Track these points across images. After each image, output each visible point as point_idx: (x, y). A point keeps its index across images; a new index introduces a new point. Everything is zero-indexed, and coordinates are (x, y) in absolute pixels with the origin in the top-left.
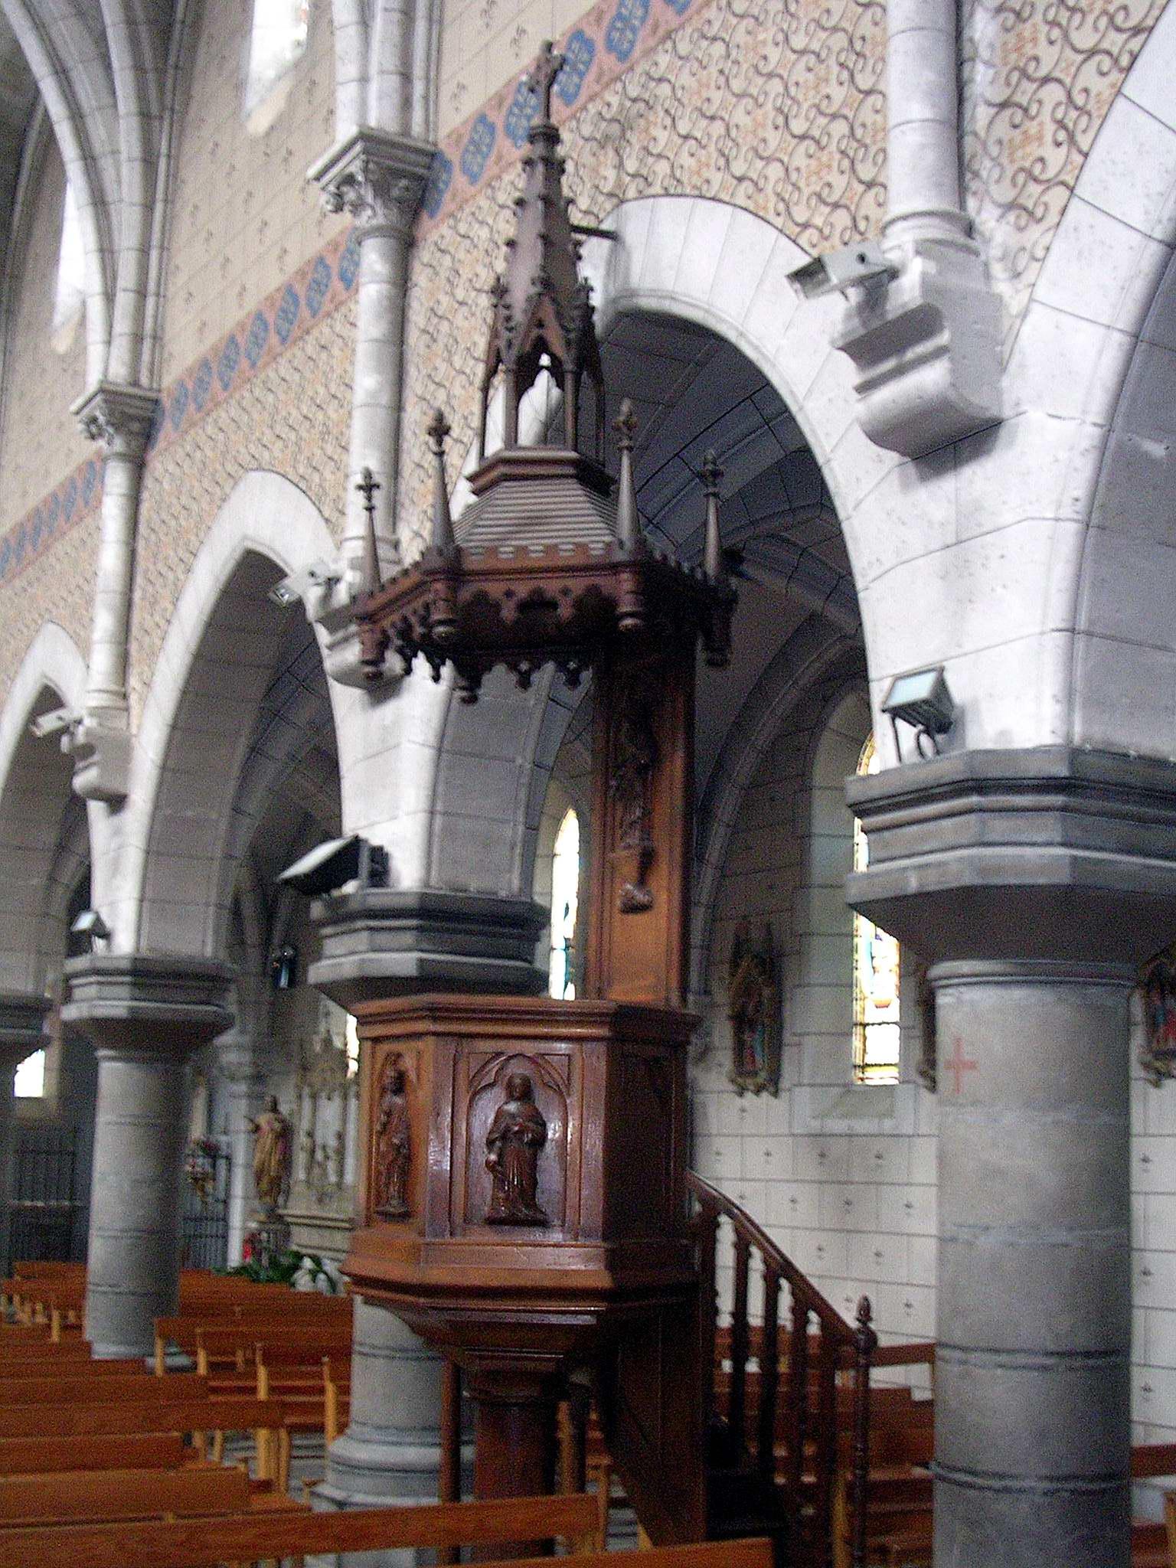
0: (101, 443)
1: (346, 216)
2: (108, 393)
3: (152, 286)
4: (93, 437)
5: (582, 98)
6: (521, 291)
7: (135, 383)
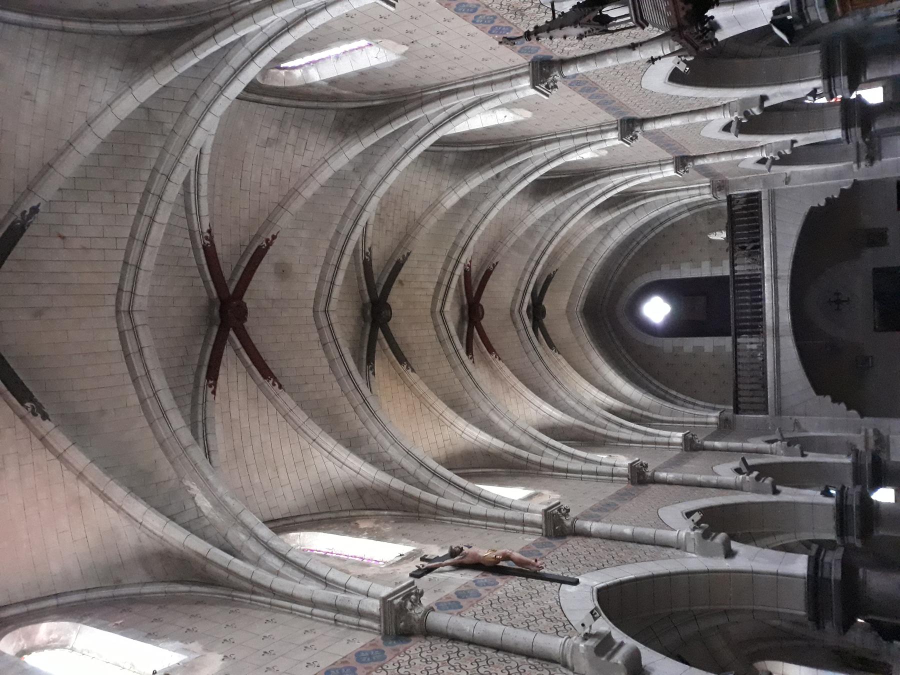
0: (638, 134)
1: (558, 84)
2: (622, 137)
3: (584, 132)
4: (637, 137)
5: (509, 25)
6: (579, 30)
7: (617, 129)
